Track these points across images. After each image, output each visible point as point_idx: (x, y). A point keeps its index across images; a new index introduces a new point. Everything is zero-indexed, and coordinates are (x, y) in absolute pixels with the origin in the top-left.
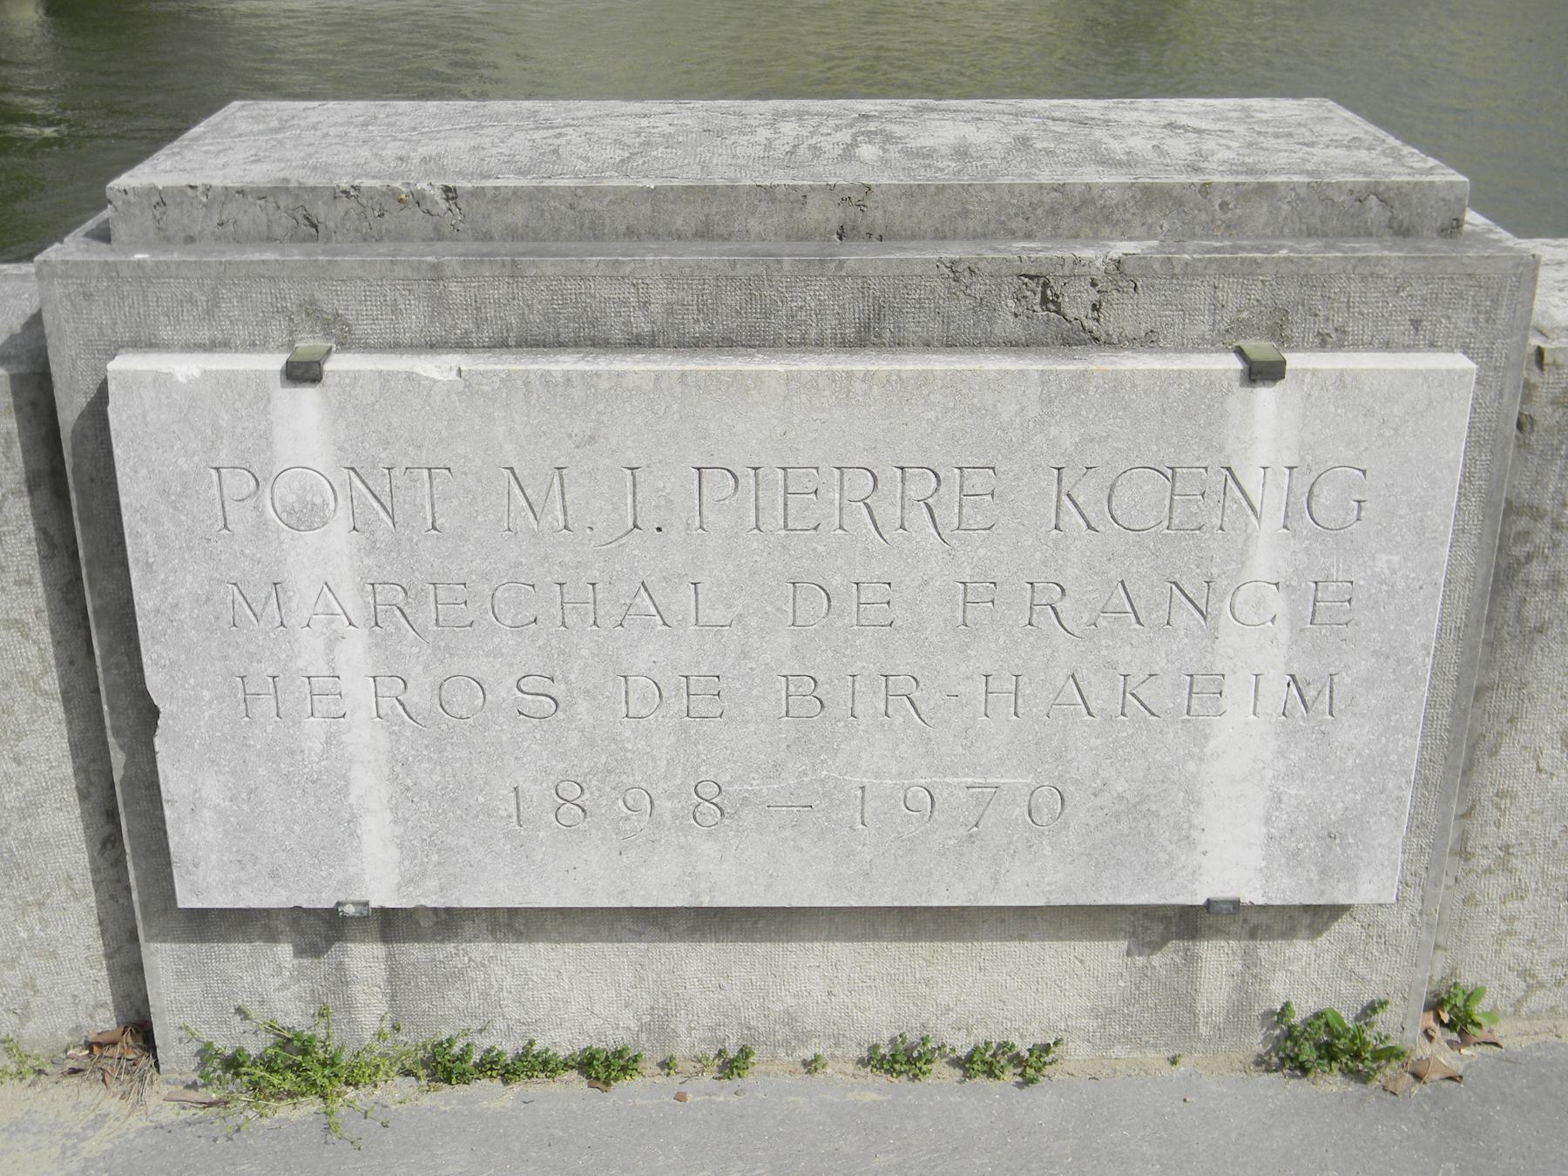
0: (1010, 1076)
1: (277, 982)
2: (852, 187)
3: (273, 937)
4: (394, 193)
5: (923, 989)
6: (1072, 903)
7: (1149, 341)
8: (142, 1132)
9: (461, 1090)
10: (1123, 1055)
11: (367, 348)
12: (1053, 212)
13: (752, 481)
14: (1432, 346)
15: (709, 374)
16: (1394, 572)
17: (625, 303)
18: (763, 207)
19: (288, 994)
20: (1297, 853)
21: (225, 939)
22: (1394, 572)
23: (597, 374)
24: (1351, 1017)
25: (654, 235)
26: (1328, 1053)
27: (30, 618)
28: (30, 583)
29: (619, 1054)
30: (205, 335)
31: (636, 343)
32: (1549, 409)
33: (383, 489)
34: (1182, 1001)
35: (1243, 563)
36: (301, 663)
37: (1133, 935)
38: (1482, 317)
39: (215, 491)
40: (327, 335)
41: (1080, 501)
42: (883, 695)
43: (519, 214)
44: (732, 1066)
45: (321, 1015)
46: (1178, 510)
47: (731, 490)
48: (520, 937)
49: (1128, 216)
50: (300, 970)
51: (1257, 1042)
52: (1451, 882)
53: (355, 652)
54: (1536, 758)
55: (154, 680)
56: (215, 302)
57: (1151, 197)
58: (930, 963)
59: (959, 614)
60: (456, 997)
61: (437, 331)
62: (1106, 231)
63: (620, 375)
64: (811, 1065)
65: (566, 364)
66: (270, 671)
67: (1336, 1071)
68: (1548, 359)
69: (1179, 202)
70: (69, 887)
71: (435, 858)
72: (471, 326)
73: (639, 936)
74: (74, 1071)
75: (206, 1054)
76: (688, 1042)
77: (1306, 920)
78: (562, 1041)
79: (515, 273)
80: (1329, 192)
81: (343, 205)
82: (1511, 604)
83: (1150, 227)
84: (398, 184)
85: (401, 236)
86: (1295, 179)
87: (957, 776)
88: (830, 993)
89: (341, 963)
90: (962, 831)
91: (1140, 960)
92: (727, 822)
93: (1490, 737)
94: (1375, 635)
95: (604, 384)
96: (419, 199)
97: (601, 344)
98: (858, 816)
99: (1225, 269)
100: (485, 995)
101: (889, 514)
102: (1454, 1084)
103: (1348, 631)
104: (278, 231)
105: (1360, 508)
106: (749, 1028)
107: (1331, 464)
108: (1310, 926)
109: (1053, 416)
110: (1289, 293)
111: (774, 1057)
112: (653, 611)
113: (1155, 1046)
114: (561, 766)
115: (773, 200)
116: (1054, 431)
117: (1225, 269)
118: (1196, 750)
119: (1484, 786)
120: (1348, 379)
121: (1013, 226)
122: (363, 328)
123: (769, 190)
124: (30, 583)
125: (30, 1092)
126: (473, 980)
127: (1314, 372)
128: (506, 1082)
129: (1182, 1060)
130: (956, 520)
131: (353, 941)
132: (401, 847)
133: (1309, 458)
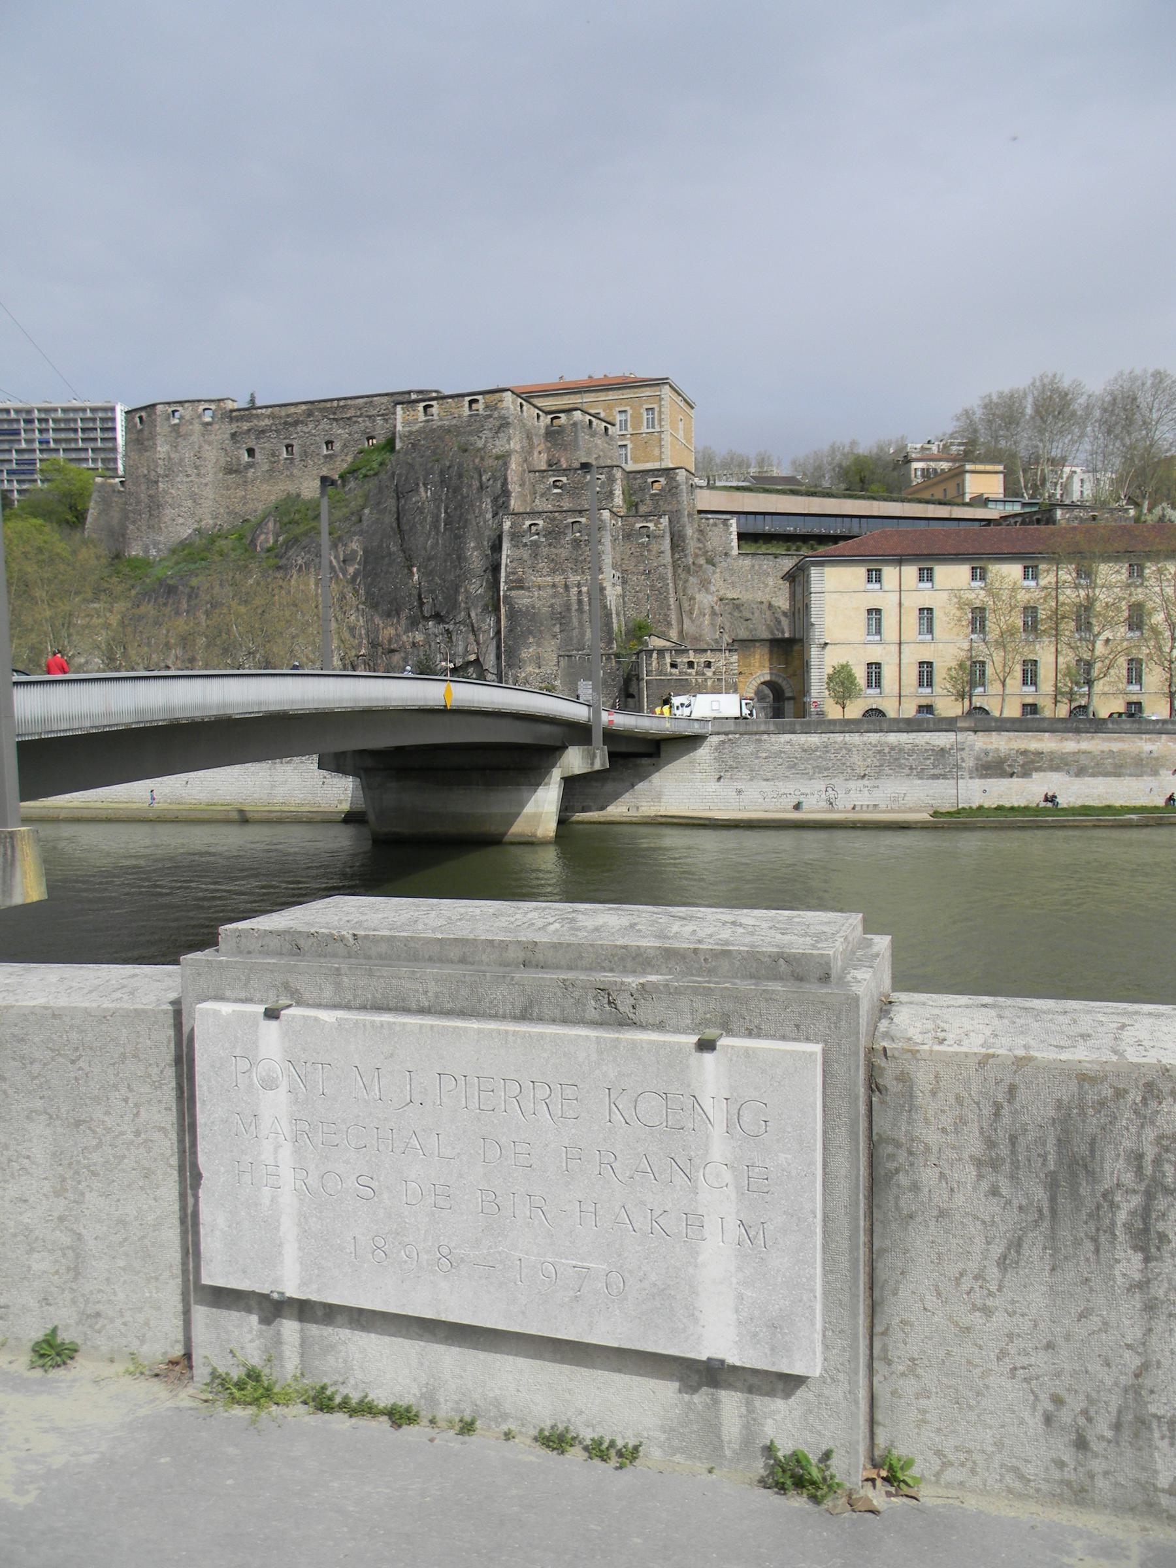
0: (614, 1461)
1: (249, 1337)
2: (528, 942)
3: (249, 1311)
4: (332, 935)
5: (567, 1396)
6: (633, 1348)
7: (660, 1027)
8: (168, 1409)
9: (327, 1416)
10: (682, 1461)
11: (308, 1005)
12: (622, 959)
13: (463, 1083)
14: (808, 1039)
15: (443, 1026)
16: (789, 1165)
17: (417, 991)
18: (489, 950)
19: (254, 1344)
20: (755, 1335)
21: (228, 1308)
22: (789, 1165)
23: (394, 1023)
24: (816, 1459)
25: (441, 960)
26: (800, 1483)
27: (169, 1127)
28: (170, 1110)
29: (408, 1410)
30: (243, 995)
31: (423, 1011)
32: (895, 1083)
33: (302, 1072)
34: (712, 1428)
35: (707, 1151)
36: (263, 1157)
37: (681, 1379)
38: (832, 1025)
39: (233, 1068)
40: (292, 998)
41: (620, 1107)
42: (528, 1207)
43: (383, 948)
44: (467, 1428)
45: (269, 1361)
46: (670, 1117)
47: (454, 1086)
48: (364, 1328)
49: (659, 963)
50: (261, 1331)
51: (759, 1467)
52: (882, 1379)
53: (286, 1151)
54: (922, 1300)
55: (202, 1159)
56: (248, 980)
57: (669, 954)
58: (571, 1380)
59: (564, 1165)
60: (331, 1360)
61: (337, 999)
62: (649, 970)
63: (404, 1024)
64: (508, 1436)
65: (387, 1018)
66: (250, 1160)
67: (805, 1495)
68: (889, 1054)
69: (684, 957)
70: (171, 1272)
71: (316, 1271)
72: (351, 998)
73: (420, 1338)
74: (157, 1375)
75: (214, 1375)
76: (444, 1411)
77: (780, 1386)
78: (382, 1398)
79: (371, 974)
80: (758, 956)
81: (312, 940)
82: (891, 1198)
83: (670, 969)
84: (334, 932)
85: (335, 955)
86: (741, 948)
87: (567, 1259)
88: (518, 1391)
89: (279, 1330)
90: (571, 1293)
91: (686, 1397)
92: (454, 1271)
93: (892, 1282)
94: (783, 1202)
95: (398, 1029)
96: (342, 938)
97: (407, 1010)
98: (518, 1276)
99: (696, 991)
100: (345, 1361)
101: (529, 1106)
102: (872, 1516)
103: (768, 1197)
104: (284, 951)
105: (766, 1126)
106: (476, 1406)
107: (747, 1099)
108: (783, 1391)
109: (604, 1060)
110: (729, 1006)
111: (489, 1428)
112: (418, 1147)
113: (700, 1458)
114: (375, 1227)
115: (494, 947)
116: (605, 1068)
117: (696, 991)
118: (692, 1260)
119: (893, 1315)
120: (751, 1052)
121: (604, 965)
122: (307, 996)
123: (491, 942)
124: (170, 1110)
125: (133, 1382)
126: (340, 1351)
127: (733, 1047)
128: (351, 1416)
129: (715, 1471)
130: (560, 1112)
131: (285, 1318)
132: (301, 1263)
133: (735, 1094)
